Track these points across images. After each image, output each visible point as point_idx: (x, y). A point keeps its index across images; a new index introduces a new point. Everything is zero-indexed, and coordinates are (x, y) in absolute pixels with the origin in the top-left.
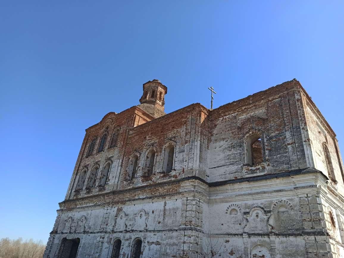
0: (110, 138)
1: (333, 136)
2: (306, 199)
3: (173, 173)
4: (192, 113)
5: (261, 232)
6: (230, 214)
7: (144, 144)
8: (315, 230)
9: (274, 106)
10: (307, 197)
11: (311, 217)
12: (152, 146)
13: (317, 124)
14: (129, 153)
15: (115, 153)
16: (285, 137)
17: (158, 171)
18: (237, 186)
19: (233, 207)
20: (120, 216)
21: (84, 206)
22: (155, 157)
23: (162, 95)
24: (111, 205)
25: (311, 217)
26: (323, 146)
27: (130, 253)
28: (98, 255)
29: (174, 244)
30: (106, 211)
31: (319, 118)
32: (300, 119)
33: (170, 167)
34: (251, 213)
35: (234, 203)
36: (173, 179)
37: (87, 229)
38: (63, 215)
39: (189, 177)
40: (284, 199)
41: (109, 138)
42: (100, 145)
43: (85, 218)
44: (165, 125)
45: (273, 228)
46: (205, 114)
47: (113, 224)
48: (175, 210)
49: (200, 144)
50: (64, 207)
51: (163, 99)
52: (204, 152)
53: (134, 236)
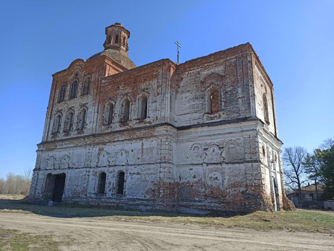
0: (81, 85)
1: (271, 85)
2: (249, 139)
3: (147, 120)
4: (162, 67)
5: (215, 162)
6: (194, 150)
7: (118, 94)
8: (252, 159)
9: (230, 65)
10: (249, 137)
11: (251, 151)
12: (127, 95)
13: (261, 79)
14: (104, 101)
15: (89, 100)
16: (237, 92)
17: (133, 118)
18: (199, 129)
19: (196, 145)
20: (102, 155)
21: (64, 146)
22: (130, 106)
23: (126, 40)
24: (92, 146)
25: (251, 151)
26: (263, 97)
27: (115, 182)
28: (86, 185)
29: (152, 174)
30: (88, 150)
31: (263, 74)
32: (249, 77)
33: (145, 115)
34: (209, 149)
35: (197, 142)
36: (148, 125)
37: (71, 166)
38: (44, 155)
39: (161, 123)
40: (233, 139)
41: (80, 86)
42: (72, 91)
43: (68, 157)
44: (137, 76)
45: (224, 159)
46: (174, 69)
47: (97, 161)
48: (151, 149)
49: (170, 96)
50: (43, 147)
51: (127, 44)
52: (173, 102)
53: (117, 169)
